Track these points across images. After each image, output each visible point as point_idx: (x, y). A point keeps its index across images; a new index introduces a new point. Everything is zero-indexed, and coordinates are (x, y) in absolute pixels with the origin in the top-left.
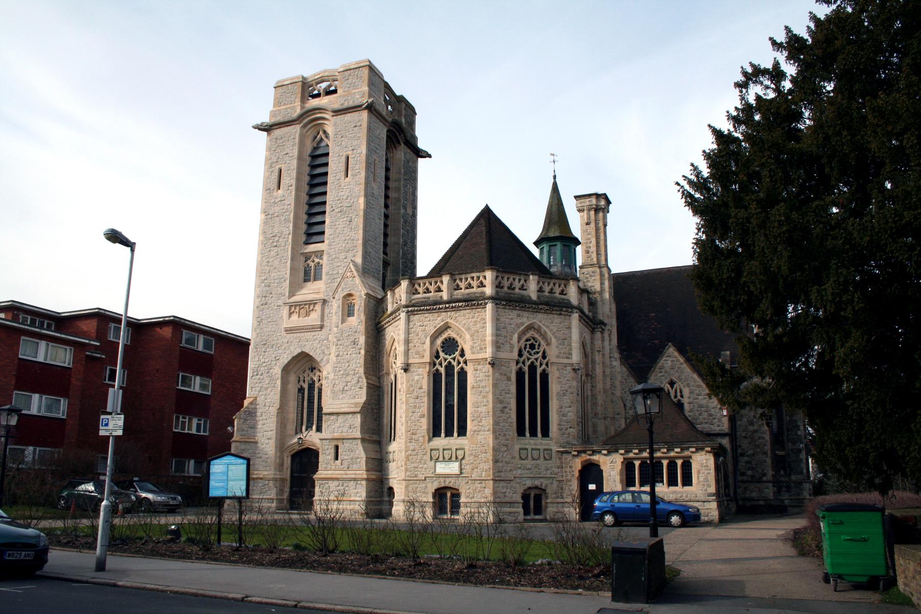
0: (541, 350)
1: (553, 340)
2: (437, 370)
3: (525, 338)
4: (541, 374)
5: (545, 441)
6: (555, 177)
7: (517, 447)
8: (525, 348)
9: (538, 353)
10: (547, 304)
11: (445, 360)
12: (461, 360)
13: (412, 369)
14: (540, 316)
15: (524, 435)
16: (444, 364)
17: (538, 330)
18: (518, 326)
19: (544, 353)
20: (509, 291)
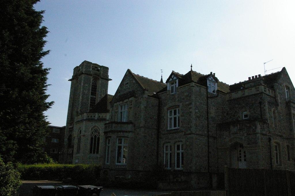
4: (97, 138)
6: (162, 76)
16: (94, 135)
19: (99, 132)
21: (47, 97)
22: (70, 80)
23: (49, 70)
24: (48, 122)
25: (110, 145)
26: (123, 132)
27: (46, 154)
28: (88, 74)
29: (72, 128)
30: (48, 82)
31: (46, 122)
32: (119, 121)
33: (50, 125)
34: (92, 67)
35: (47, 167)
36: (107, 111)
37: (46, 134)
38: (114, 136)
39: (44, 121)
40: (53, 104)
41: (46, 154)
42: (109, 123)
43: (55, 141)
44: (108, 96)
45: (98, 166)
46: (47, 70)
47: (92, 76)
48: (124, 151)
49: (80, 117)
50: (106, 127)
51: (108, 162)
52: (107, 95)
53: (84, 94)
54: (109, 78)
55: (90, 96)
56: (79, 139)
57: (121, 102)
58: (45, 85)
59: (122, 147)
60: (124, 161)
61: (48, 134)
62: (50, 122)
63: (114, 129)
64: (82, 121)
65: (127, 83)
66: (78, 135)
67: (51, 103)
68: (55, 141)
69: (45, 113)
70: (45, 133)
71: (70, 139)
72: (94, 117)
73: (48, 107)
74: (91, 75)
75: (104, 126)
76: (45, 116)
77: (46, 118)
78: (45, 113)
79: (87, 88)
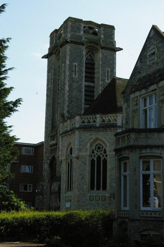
0: (104, 149)
1: (108, 144)
2: (93, 159)
3: (95, 144)
4: (103, 161)
5: (104, 192)
7: (89, 195)
8: (95, 149)
9: (102, 151)
10: (103, 127)
11: (97, 154)
12: (105, 155)
13: (79, 159)
14: (101, 133)
15: (94, 189)
16: (96, 156)
17: (101, 140)
18: (90, 139)
19: (105, 150)
20: (88, 124)
21: (7, 91)
22: (44, 57)
23: (8, 41)
24: (13, 137)
25: (127, 173)
26: (151, 147)
27: (12, 194)
28: (77, 42)
29: (56, 144)
30: (8, 64)
31: (10, 137)
32: (142, 127)
33: (18, 141)
34: (83, 27)
35: (17, 219)
36: (117, 110)
37: (11, 159)
38: (133, 156)
39: (7, 136)
40: (20, 104)
41: (12, 194)
42: (122, 133)
43: (26, 169)
44: (117, 81)
45: (107, 213)
46: (4, 42)
47: (84, 45)
48: (155, 183)
49: (68, 125)
50: (117, 140)
51: (125, 205)
52: (114, 80)
53: (72, 80)
54: (117, 46)
55: (84, 83)
56: (70, 165)
57: (143, 91)
58: (3, 69)
59: (152, 176)
60: (155, 202)
61: (16, 158)
62: (17, 137)
63: (131, 141)
64: (72, 130)
65: (154, 54)
66: (66, 156)
67: (17, 103)
68: (26, 169)
69: (8, 121)
70: (11, 156)
71: (53, 163)
72: (94, 121)
73: (11, 110)
74: (83, 44)
75: (114, 139)
76: (8, 126)
77: (9, 129)
78: (8, 121)
79: (77, 69)
